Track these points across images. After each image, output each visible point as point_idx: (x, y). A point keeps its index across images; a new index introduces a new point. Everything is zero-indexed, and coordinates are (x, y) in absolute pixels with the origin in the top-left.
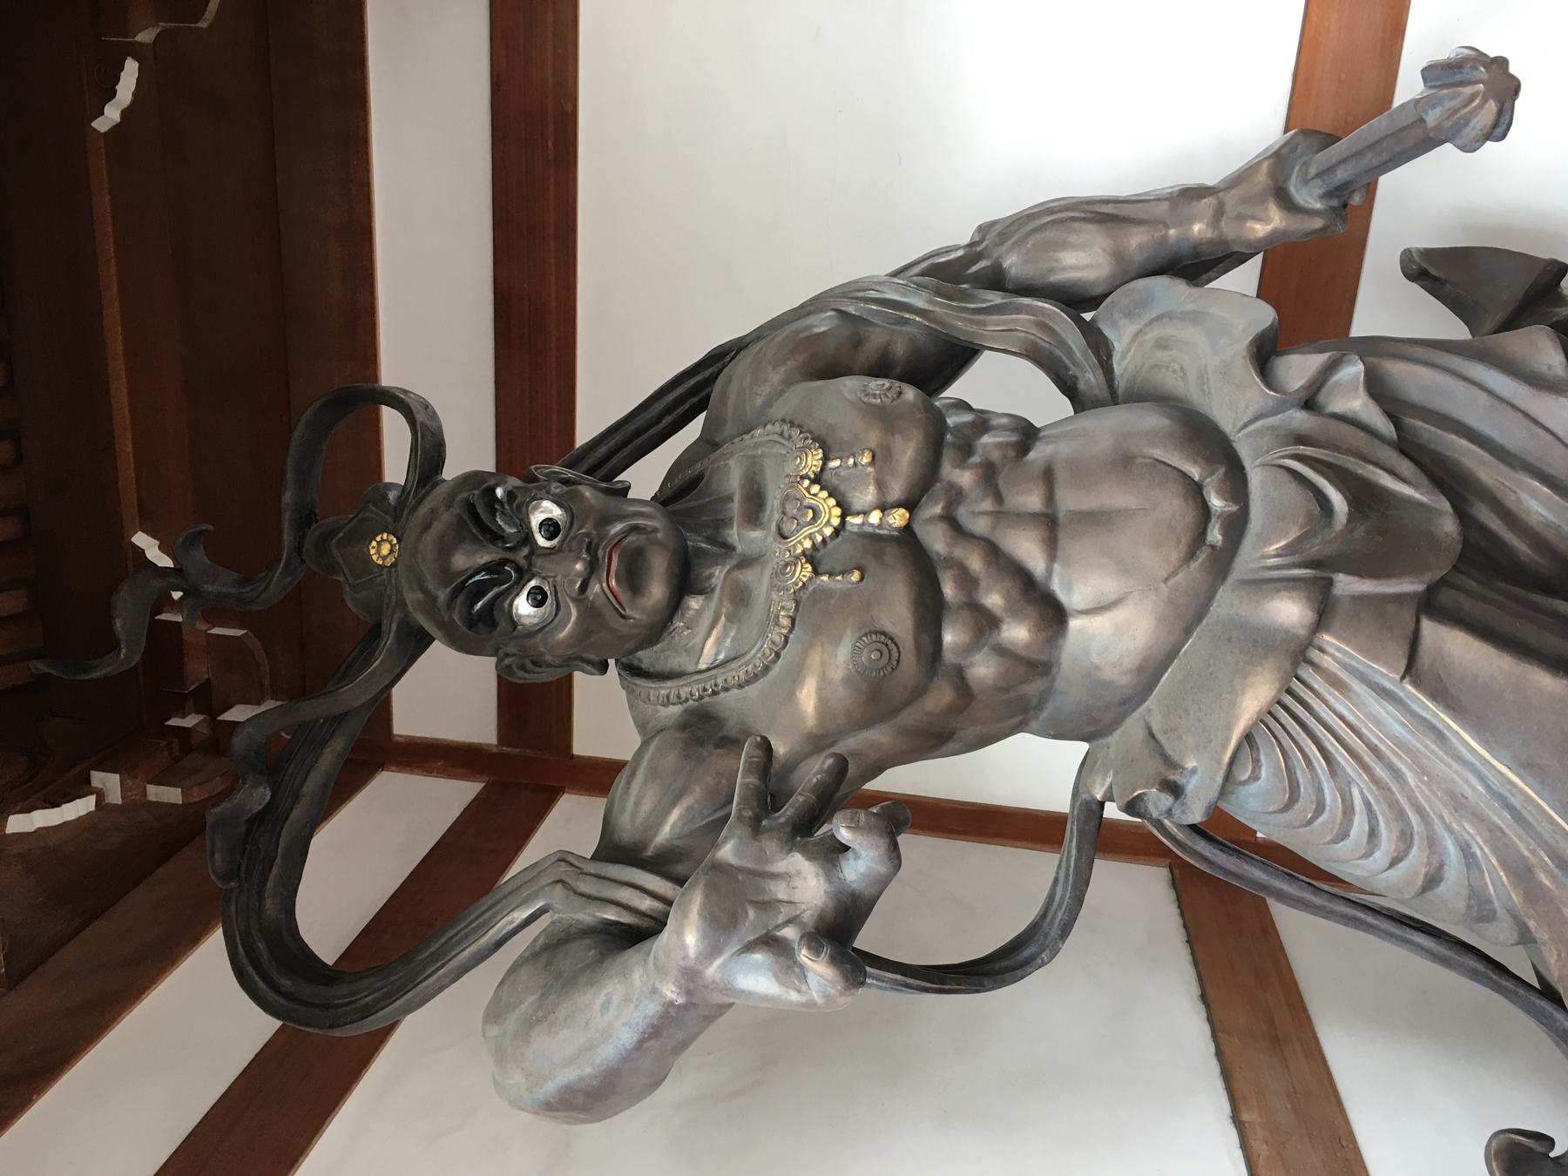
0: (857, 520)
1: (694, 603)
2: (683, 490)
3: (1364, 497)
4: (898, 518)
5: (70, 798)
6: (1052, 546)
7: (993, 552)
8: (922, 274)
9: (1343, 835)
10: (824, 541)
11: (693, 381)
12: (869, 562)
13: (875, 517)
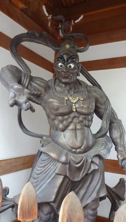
0: (74, 105)
1: (64, 86)
2: (79, 82)
3: (80, 169)
4: (74, 110)
5: (48, 13)
6: (72, 130)
7: (71, 122)
8: (112, 112)
9: (39, 167)
10: (71, 101)
11: (96, 84)
12: (68, 107)
13: (74, 107)
